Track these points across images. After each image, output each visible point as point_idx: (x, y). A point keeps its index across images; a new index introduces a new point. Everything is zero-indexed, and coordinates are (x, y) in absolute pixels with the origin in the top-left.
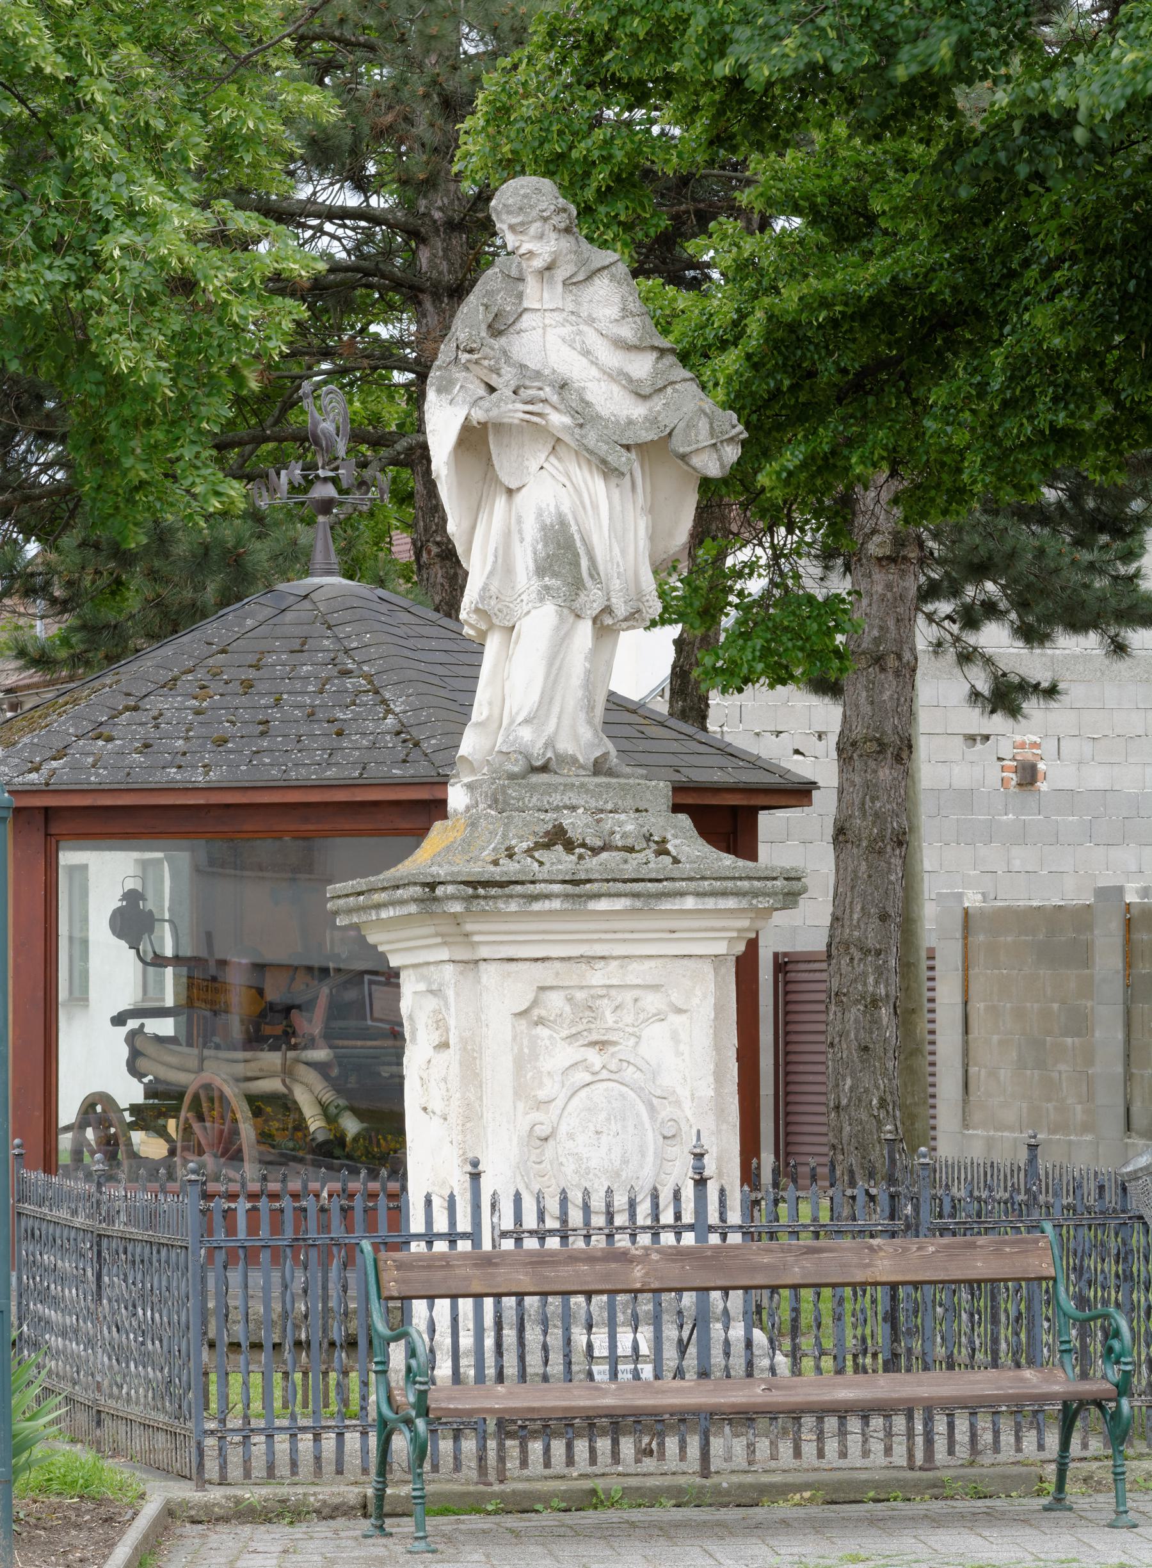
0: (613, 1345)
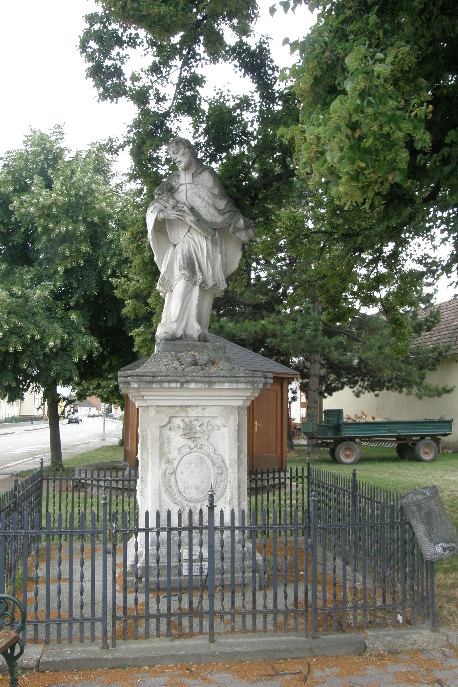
0: (190, 554)
